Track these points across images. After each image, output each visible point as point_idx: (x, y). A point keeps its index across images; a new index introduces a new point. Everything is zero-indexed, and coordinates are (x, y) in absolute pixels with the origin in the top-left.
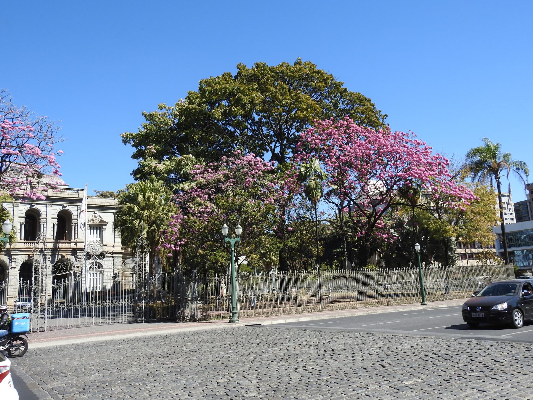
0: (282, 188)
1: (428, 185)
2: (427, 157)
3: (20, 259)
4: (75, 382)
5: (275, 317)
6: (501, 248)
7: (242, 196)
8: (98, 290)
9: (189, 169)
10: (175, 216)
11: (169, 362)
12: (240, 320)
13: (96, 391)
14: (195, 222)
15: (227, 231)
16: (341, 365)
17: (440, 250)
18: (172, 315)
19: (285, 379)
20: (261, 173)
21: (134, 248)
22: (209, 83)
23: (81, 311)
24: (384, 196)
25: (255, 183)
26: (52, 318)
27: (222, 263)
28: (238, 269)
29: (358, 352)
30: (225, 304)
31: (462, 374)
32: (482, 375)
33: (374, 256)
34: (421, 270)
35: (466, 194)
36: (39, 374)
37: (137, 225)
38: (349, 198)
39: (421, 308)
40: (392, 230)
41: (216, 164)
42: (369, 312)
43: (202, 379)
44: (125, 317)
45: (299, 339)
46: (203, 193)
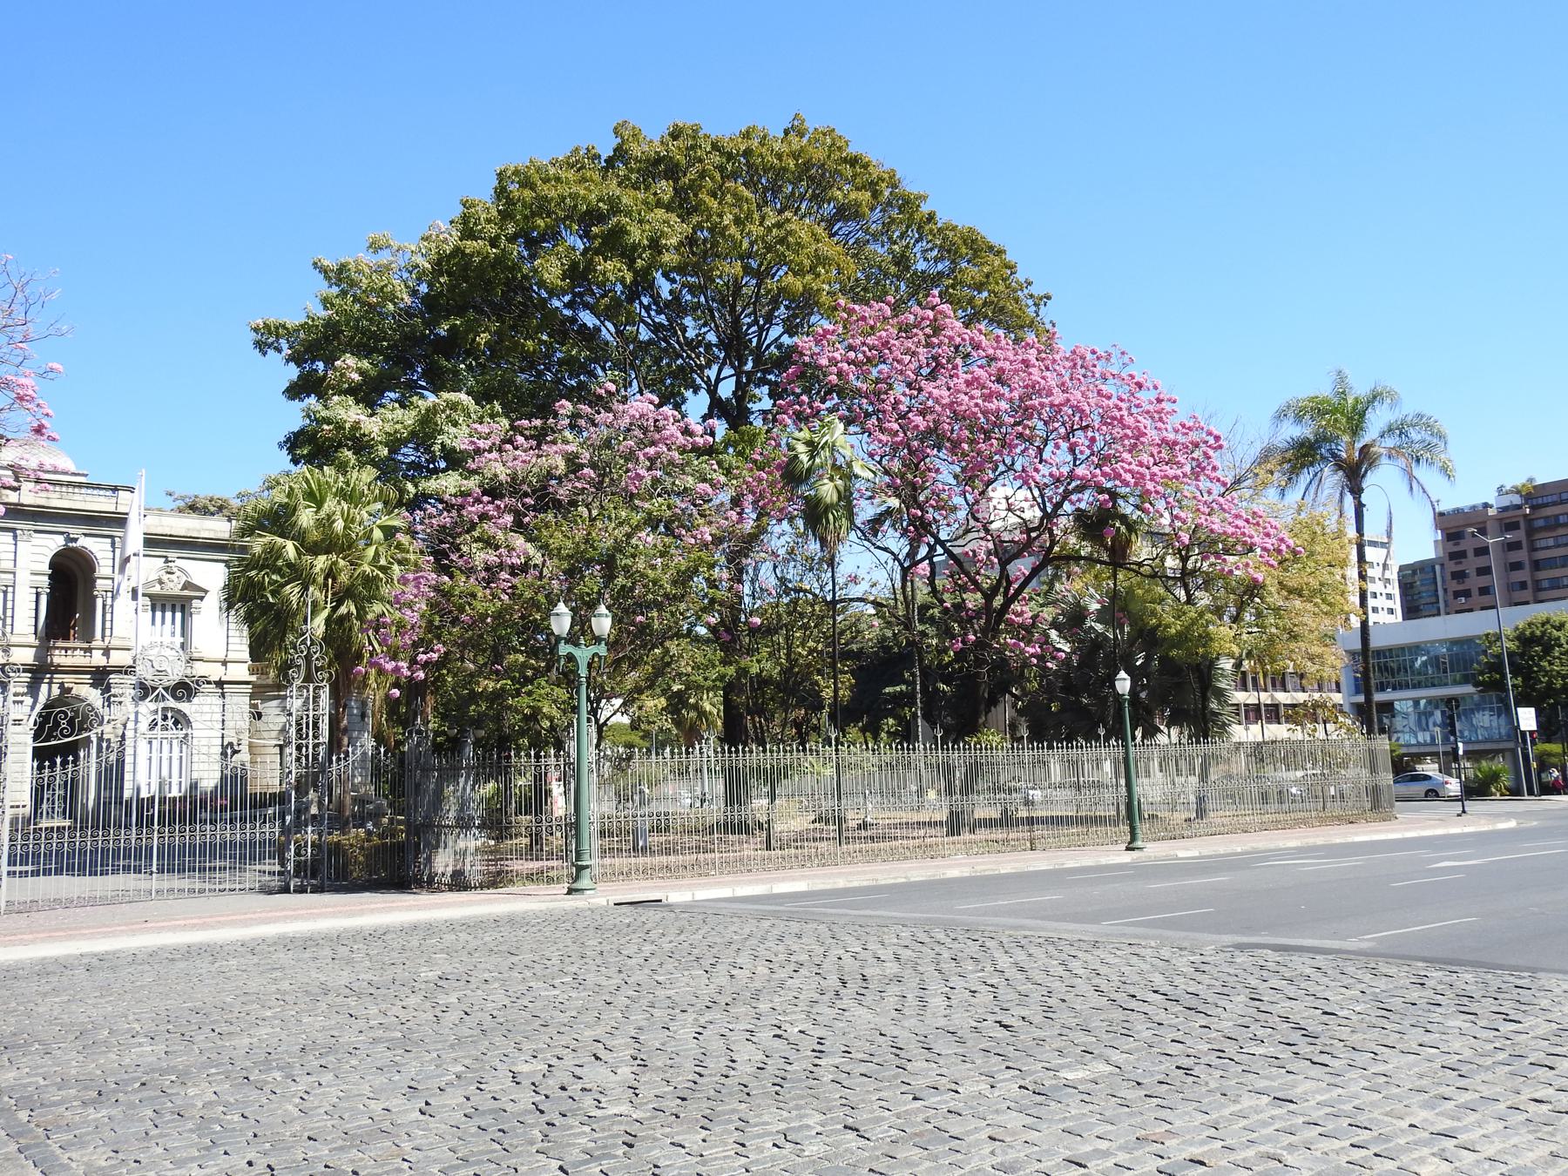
0: (736, 502)
1: (1161, 505)
2: (1160, 425)
4: (73, 1072)
5: (704, 880)
6: (1357, 692)
7: (621, 524)
8: (175, 793)
9: (457, 437)
10: (411, 576)
11: (374, 1010)
12: (600, 886)
13: (135, 1098)
14: (473, 596)
15: (566, 622)
16: (883, 1022)
17: (1183, 693)
18: (397, 869)
19: (717, 1064)
20: (676, 455)
21: (285, 668)
22: (527, 178)
23: (116, 855)
24: (1034, 535)
25: (656, 481)
26: (24, 874)
27: (551, 719)
28: (600, 738)
29: (935, 985)
30: (557, 840)
31: (1231, 1049)
32: (1285, 1054)
33: (1000, 708)
34: (1132, 750)
35: (1268, 535)
37: (294, 599)
38: (933, 535)
39: (1128, 857)
40: (1053, 634)
41: (538, 422)
42: (978, 868)
43: (467, 1062)
44: (252, 874)
45: (768, 944)
46: (498, 507)
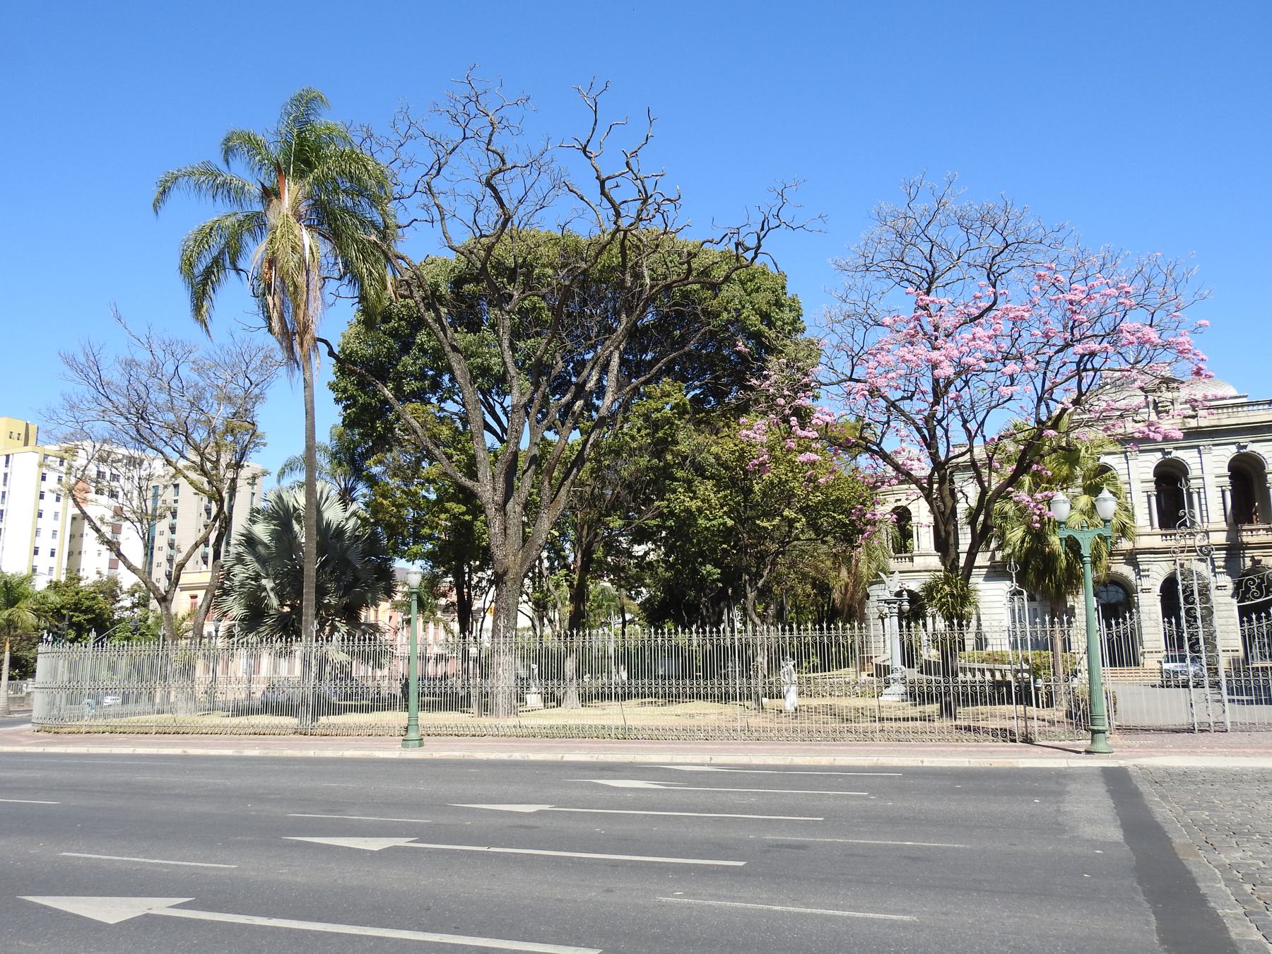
3: (1157, 572)
36: (1205, 827)
